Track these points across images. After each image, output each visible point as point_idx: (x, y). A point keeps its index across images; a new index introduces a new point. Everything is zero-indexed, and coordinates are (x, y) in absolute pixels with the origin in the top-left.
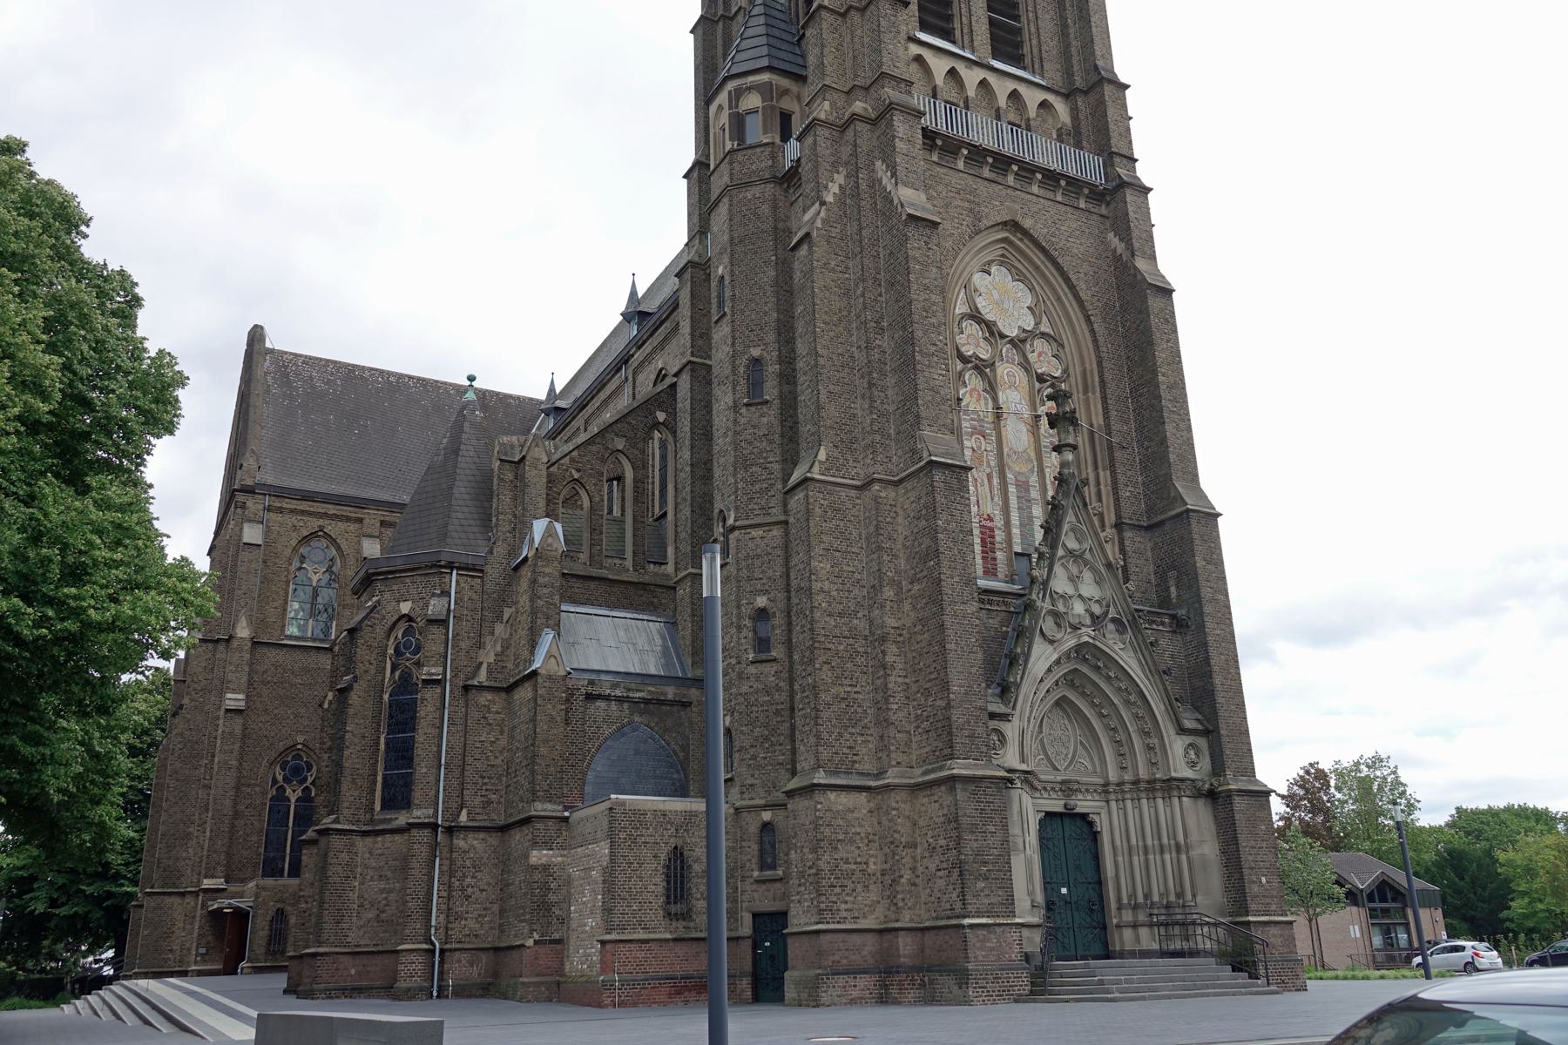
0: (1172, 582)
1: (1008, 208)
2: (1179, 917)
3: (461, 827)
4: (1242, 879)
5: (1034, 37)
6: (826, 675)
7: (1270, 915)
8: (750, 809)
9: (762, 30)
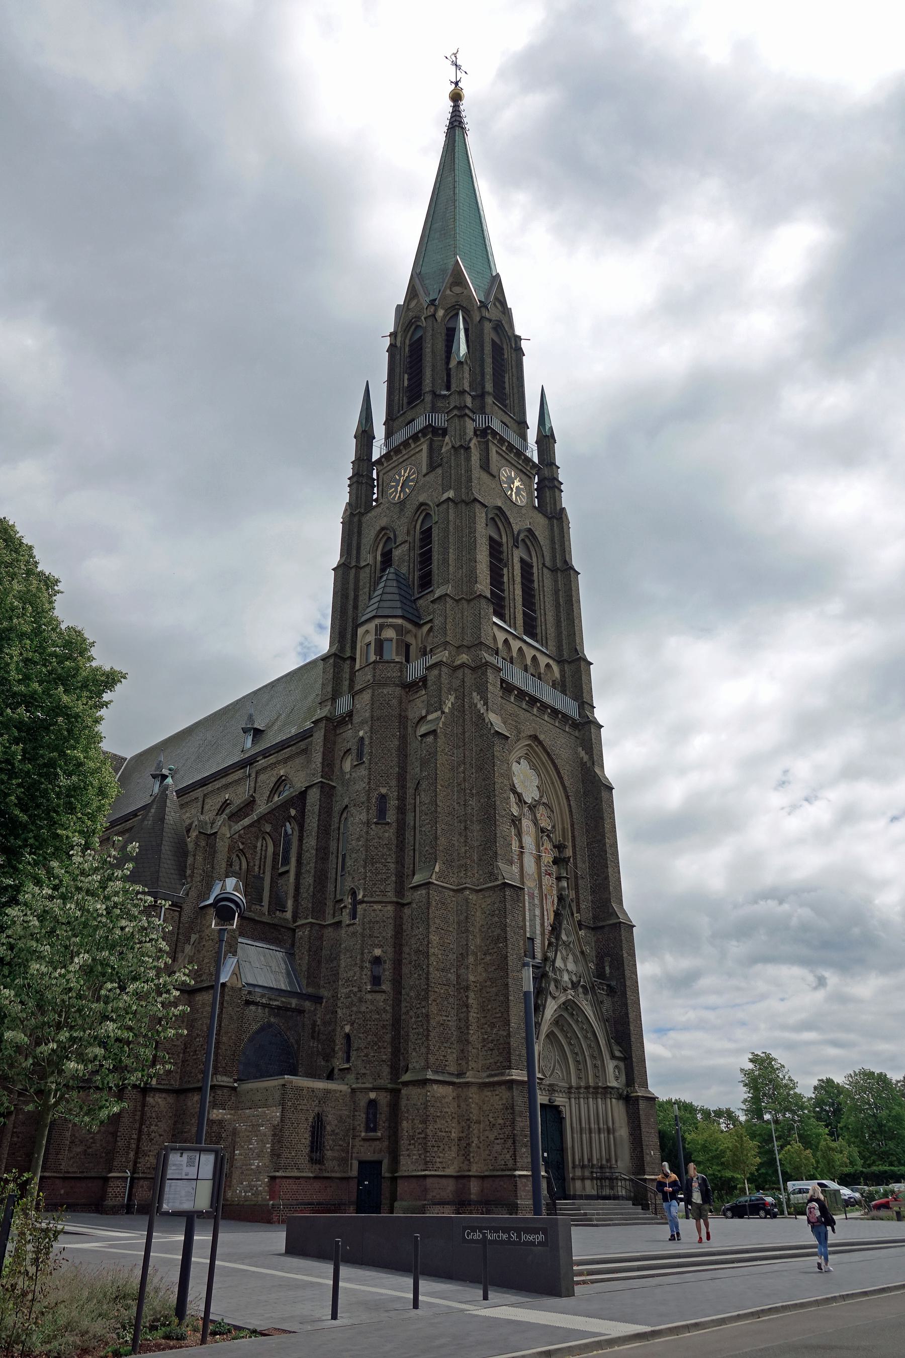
0: (607, 964)
1: (534, 727)
2: (608, 1174)
3: (153, 1088)
4: (642, 1151)
5: (543, 624)
6: (434, 1009)
8: (362, 1090)
9: (395, 590)
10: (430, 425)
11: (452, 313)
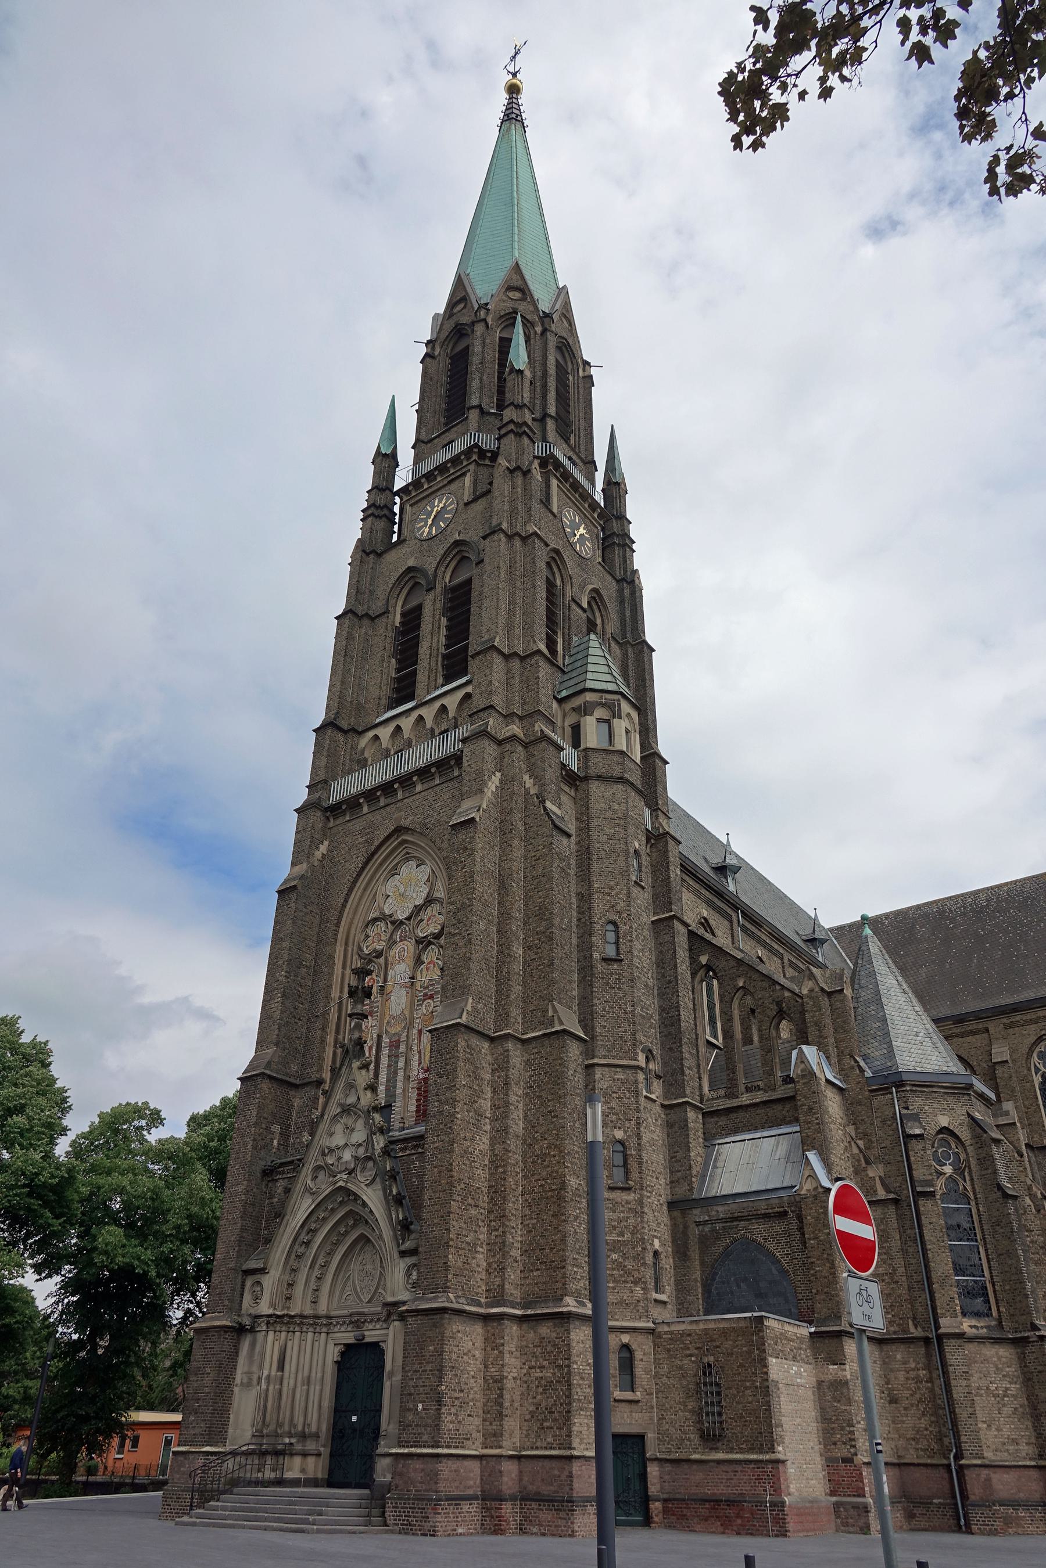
7: (420, 1447)
10: (476, 445)
11: (509, 320)
